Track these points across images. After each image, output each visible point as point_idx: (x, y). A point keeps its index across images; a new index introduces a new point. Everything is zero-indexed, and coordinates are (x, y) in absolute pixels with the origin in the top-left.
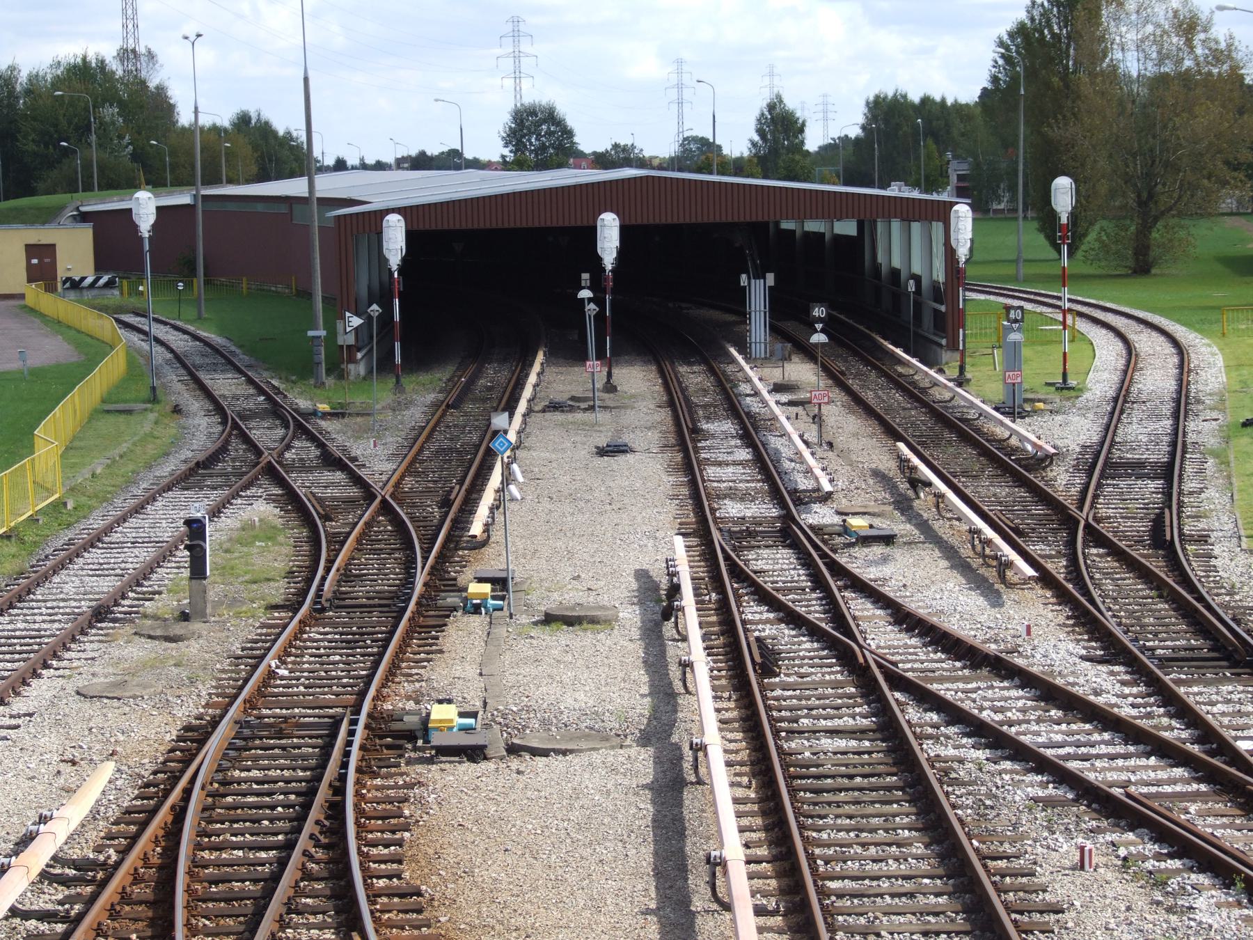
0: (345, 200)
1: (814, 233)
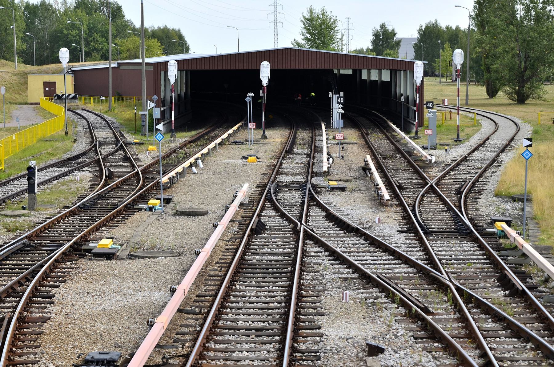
1: (374, 80)
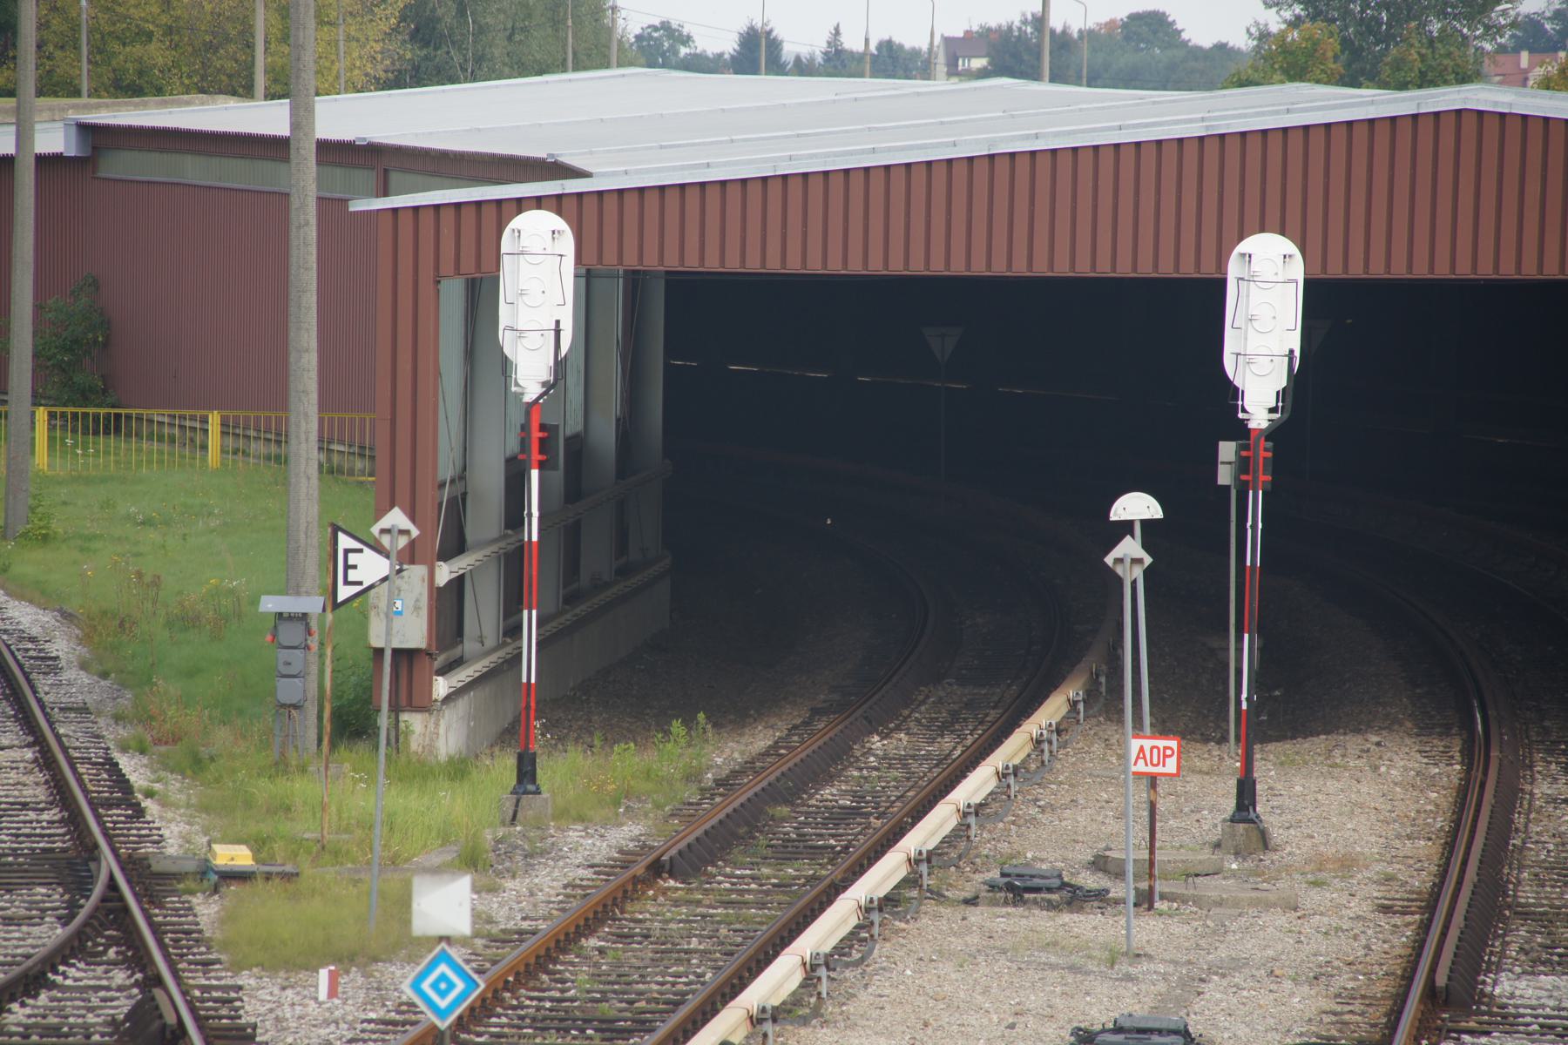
0: (444, 156)
